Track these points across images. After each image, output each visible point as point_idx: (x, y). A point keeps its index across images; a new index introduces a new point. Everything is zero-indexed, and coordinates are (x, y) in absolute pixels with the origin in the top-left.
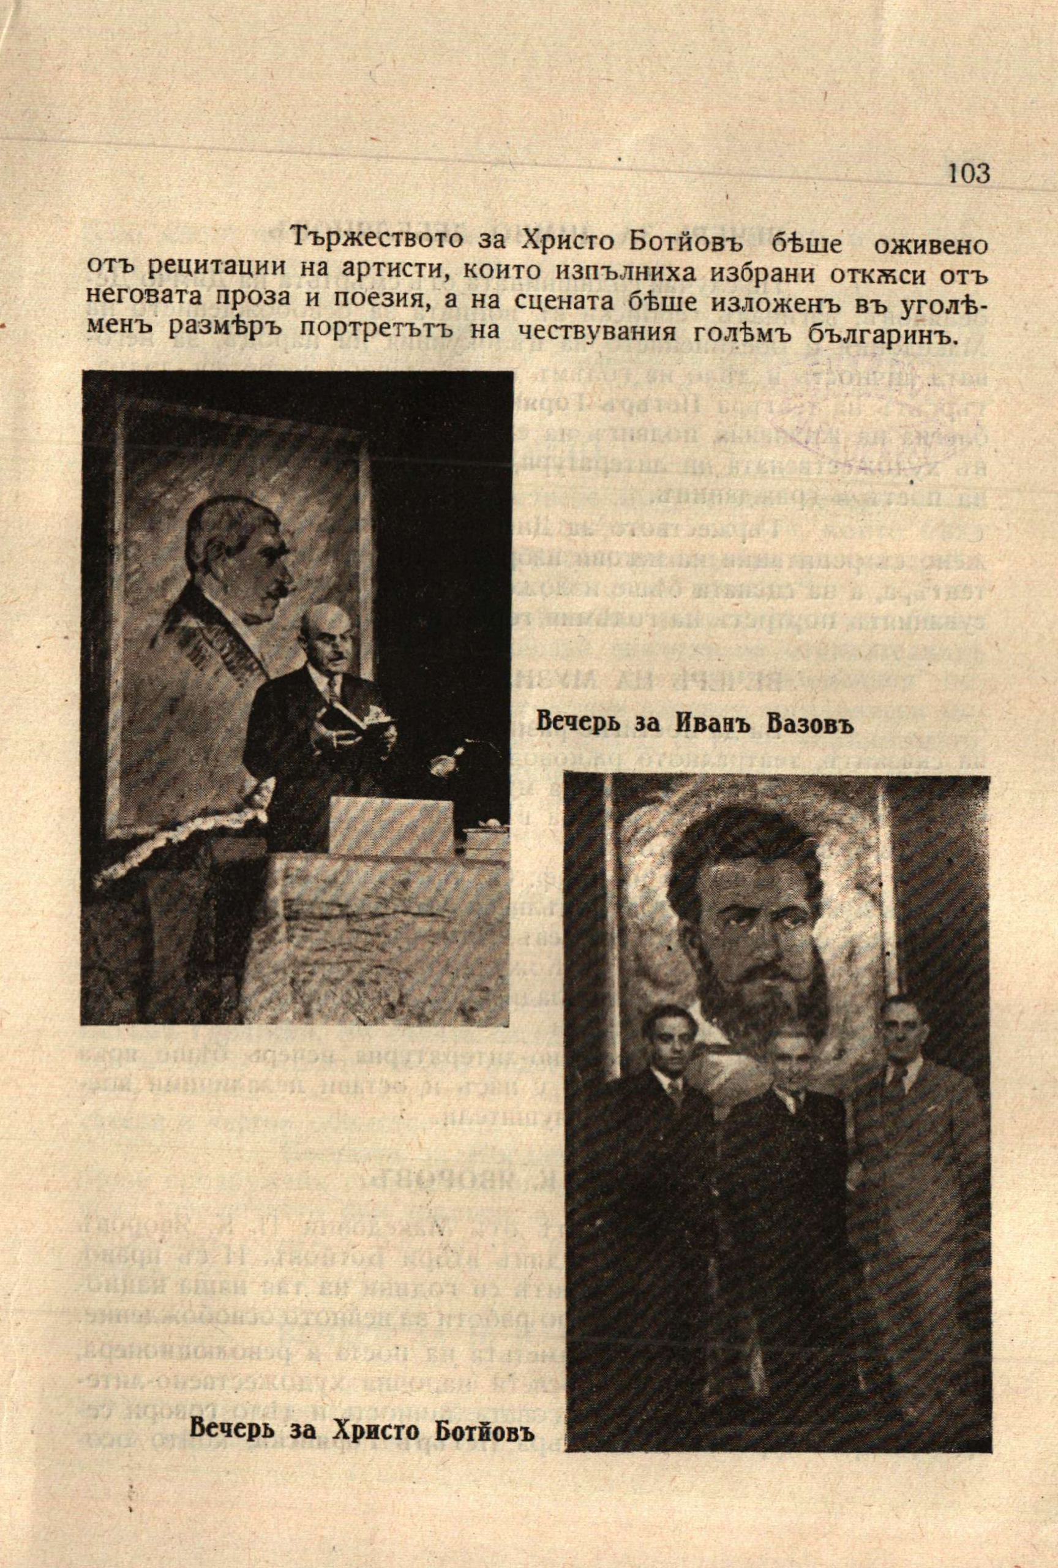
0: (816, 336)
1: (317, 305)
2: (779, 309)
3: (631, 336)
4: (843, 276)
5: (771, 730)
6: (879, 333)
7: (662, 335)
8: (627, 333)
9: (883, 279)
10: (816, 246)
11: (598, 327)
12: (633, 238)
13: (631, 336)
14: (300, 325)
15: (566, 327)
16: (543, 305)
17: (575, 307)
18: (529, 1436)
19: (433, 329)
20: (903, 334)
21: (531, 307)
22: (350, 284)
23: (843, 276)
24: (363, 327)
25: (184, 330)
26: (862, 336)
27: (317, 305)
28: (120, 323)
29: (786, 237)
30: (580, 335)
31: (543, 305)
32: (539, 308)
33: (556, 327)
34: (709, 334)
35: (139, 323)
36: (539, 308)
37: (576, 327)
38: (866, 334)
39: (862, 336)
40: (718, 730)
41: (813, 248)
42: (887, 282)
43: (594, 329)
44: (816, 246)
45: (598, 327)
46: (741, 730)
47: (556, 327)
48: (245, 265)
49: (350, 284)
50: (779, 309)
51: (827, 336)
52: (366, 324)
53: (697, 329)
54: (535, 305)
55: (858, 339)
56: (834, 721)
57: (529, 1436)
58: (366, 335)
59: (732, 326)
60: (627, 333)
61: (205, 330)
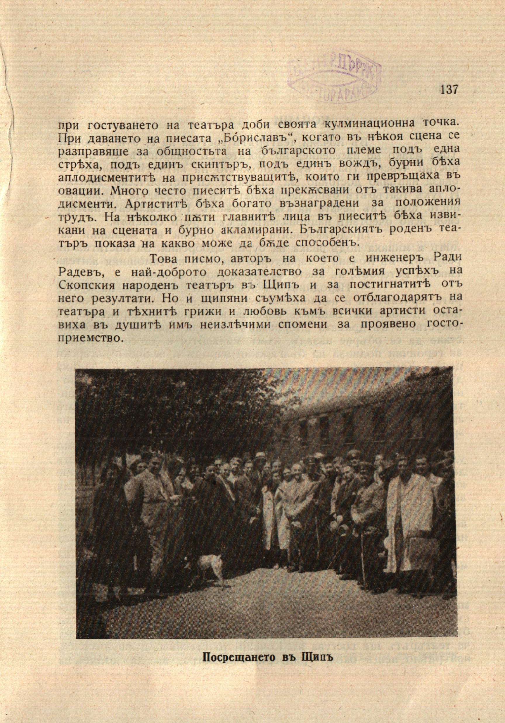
0: (235, 204)
1: (422, 165)
2: (221, 245)
3: (114, 140)
4: (191, 273)
5: (284, 660)
6: (134, 298)
7: (454, 202)
8: (140, 126)
9: (269, 245)
10: (413, 176)
11: (128, 323)
12: (301, 228)
13: (275, 231)
14: (361, 323)
15: (104, 336)
16: (125, 232)
17: (130, 288)
18: (331, 659)
19: (453, 283)
20: (320, 176)
21: (120, 233)
22: (285, 198)
23: (191, 273)
24: (320, 203)
25: (92, 154)
26: (386, 284)
27: (422, 165)
28: (396, 257)
29: (400, 213)
30: (241, 179)
31: (125, 232)
32: (123, 233)
33: (99, 336)
34: (434, 324)
35: (320, 310)
36: (123, 233)
37: (108, 336)
38: (326, 229)
39: (386, 284)
40: (250, 660)
41: (412, 177)
42: (271, 246)
43: (126, 324)
44: (413, 176)
45: (128, 323)
46: (291, 660)
47: (99, 336)
48: (415, 175)
49: (285, 198)
50: (221, 245)
51: (269, 151)
52: (191, 310)
53: (186, 310)
54: (122, 232)
55: (323, 231)
56: (287, 656)
57: (331, 659)
58: (72, 168)
59: (411, 146)
60: (140, 126)
61: (74, 153)
